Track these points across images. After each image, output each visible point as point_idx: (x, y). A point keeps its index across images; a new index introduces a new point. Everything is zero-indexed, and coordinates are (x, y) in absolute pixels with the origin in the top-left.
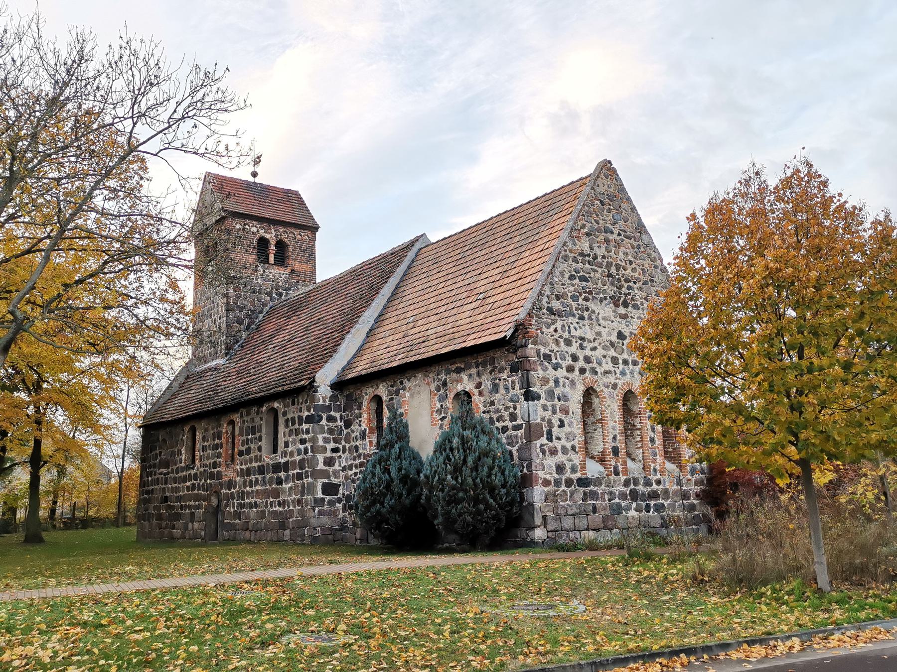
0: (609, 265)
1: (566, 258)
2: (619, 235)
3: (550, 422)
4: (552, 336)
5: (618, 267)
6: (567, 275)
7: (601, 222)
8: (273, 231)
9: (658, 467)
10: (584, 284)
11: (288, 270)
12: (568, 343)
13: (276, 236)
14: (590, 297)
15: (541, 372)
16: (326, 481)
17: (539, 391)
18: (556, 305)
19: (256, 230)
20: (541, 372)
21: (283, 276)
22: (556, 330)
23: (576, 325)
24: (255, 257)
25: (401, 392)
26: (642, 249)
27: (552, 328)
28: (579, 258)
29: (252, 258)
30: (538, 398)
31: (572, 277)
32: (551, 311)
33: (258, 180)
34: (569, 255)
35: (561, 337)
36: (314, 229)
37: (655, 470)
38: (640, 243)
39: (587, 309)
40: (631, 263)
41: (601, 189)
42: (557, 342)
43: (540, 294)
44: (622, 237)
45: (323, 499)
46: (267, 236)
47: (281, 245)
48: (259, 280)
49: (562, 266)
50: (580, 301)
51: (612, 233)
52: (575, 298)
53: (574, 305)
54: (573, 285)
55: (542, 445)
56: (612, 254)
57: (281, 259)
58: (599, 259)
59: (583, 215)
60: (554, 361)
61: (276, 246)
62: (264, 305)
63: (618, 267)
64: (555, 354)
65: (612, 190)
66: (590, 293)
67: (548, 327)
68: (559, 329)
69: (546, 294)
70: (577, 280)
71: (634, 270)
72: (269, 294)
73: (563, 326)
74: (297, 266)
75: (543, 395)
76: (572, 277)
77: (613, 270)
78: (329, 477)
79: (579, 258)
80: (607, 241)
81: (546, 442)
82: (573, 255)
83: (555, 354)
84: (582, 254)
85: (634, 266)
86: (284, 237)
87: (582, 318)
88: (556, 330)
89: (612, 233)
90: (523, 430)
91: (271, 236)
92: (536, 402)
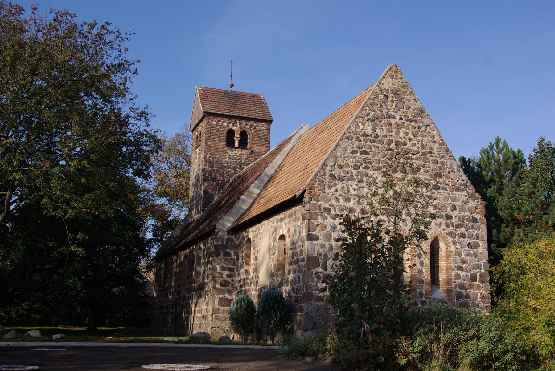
0: (390, 142)
1: (349, 138)
2: (401, 119)
3: (326, 255)
4: (333, 195)
5: (397, 143)
6: (349, 151)
7: (384, 110)
8: (238, 124)
9: (424, 292)
10: (364, 156)
11: (249, 152)
12: (348, 200)
13: (241, 128)
14: (370, 166)
15: (320, 220)
16: (221, 296)
17: (318, 235)
18: (337, 172)
19: (226, 124)
20: (320, 220)
21: (245, 156)
22: (336, 191)
23: (354, 186)
24: (225, 143)
25: (259, 235)
26: (423, 129)
27: (333, 189)
28: (362, 138)
29: (223, 144)
30: (317, 239)
31: (354, 152)
32: (333, 177)
33: (233, 89)
34: (353, 135)
35: (341, 195)
36: (270, 122)
37: (421, 294)
38: (421, 125)
39: (367, 175)
40: (410, 140)
41: (386, 86)
42: (337, 200)
43: (324, 164)
44: (403, 121)
45: (219, 309)
46: (234, 128)
47: (244, 135)
48: (227, 159)
49: (345, 144)
50: (361, 169)
51: (394, 118)
52: (357, 168)
53: (354, 172)
54: (355, 158)
55: (317, 273)
56: (393, 134)
57: (243, 144)
58: (380, 138)
59: (368, 106)
60: (333, 213)
61: (240, 134)
62: (231, 176)
63: (397, 143)
64: (335, 208)
65: (396, 86)
66: (370, 163)
67: (330, 187)
68: (339, 190)
69: (329, 165)
70: (358, 154)
71: (414, 145)
72: (234, 169)
73: (343, 187)
74: (256, 148)
75: (321, 237)
76: (354, 152)
77: (393, 145)
78: (224, 294)
79: (362, 138)
80: (390, 124)
81: (321, 270)
82: (356, 136)
83: (335, 208)
84: (366, 135)
85: (413, 142)
86: (247, 129)
87: (361, 181)
88: (336, 191)
89: (394, 118)
90: (305, 262)
91: (237, 128)
92: (315, 242)
